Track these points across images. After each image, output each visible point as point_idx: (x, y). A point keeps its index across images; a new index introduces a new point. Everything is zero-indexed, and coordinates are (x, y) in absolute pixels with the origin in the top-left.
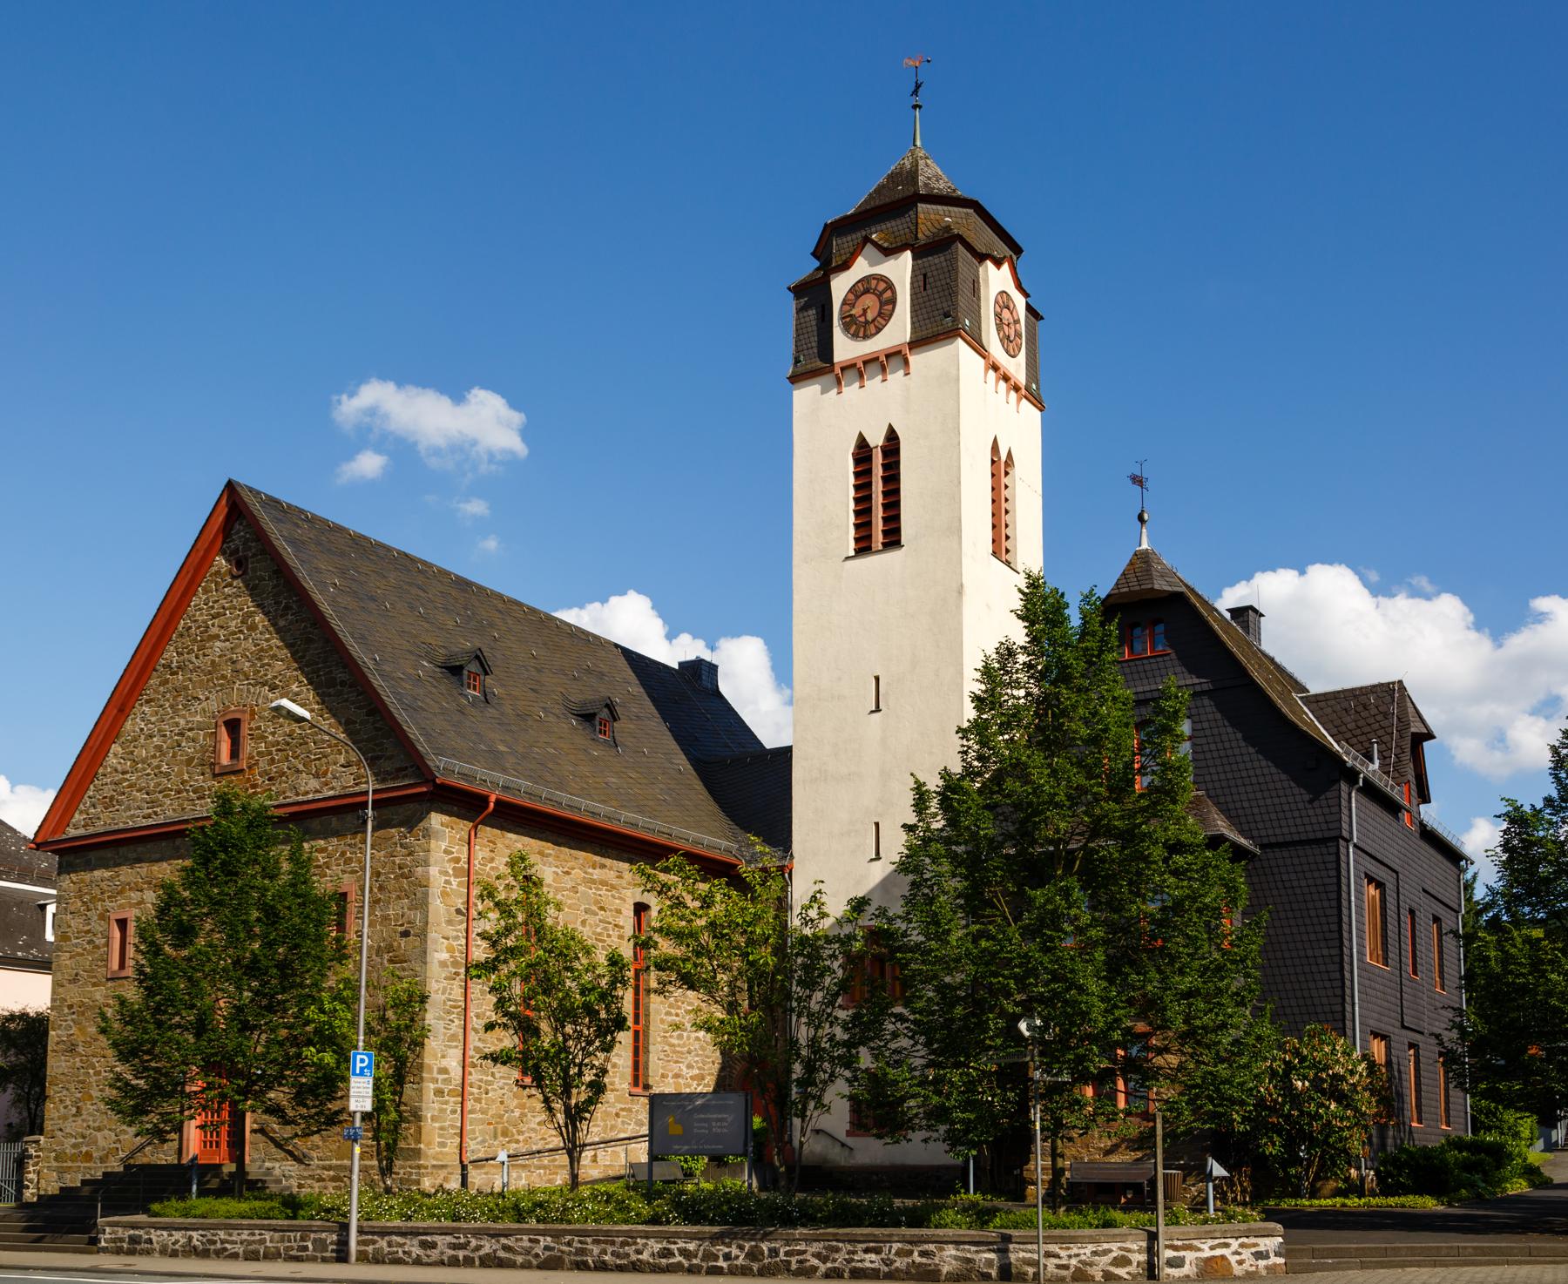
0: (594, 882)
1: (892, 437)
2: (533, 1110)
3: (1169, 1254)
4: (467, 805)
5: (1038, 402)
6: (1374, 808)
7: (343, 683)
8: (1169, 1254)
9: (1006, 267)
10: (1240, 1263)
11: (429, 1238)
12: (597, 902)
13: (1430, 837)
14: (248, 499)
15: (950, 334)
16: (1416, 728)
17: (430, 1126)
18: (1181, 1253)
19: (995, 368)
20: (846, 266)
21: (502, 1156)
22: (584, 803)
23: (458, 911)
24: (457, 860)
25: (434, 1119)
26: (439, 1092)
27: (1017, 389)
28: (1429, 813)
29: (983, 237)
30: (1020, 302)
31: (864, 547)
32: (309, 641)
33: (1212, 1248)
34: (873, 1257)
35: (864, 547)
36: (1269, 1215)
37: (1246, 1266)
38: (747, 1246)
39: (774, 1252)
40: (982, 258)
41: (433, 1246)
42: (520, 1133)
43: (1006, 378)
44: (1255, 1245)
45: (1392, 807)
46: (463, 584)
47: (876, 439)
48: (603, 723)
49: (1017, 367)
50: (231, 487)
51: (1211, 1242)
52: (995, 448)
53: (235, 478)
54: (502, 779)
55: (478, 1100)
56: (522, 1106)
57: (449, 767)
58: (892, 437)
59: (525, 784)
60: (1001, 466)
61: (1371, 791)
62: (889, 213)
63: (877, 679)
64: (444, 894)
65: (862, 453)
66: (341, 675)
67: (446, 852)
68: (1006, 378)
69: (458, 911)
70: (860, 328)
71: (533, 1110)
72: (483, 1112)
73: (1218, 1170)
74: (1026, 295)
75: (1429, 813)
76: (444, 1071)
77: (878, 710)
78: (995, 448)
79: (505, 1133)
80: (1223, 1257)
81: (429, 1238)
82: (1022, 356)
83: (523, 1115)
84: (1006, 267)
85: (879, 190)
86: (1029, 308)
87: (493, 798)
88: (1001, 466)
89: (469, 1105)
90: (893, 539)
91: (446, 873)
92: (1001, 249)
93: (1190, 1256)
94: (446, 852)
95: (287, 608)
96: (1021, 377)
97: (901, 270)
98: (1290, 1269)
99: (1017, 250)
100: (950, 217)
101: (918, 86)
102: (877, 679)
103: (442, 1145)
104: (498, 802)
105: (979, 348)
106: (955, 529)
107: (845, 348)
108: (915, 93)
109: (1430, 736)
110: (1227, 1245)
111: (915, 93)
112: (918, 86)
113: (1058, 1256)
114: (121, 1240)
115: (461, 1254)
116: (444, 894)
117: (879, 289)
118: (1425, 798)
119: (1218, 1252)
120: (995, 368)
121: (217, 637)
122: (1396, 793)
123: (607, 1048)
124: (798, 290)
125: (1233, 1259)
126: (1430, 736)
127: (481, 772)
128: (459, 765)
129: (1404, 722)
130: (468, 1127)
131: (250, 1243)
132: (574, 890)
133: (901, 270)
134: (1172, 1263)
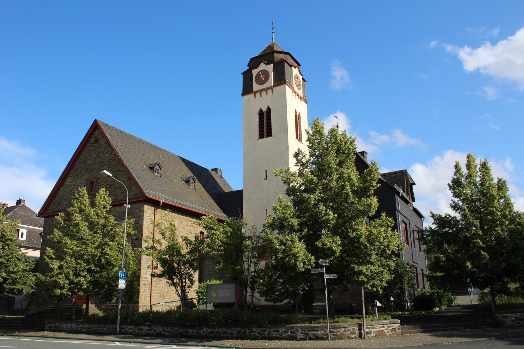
0: (189, 226)
1: (269, 109)
2: (171, 290)
3: (367, 330)
4: (155, 204)
5: (306, 101)
6: (403, 202)
7: (122, 171)
8: (367, 330)
9: (297, 68)
10: (388, 332)
11: (505, 315)
12: (189, 231)
13: (415, 210)
14: (99, 123)
15: (284, 83)
16: (411, 182)
17: (141, 294)
18: (371, 330)
19: (295, 92)
20: (257, 67)
21: (162, 303)
22: (186, 204)
23: (151, 233)
24: (151, 219)
25: (143, 292)
26: (145, 284)
27: (301, 98)
28: (415, 205)
29: (291, 62)
30: (301, 77)
31: (261, 136)
32: (114, 160)
33: (379, 328)
34: (276, 333)
35: (261, 136)
36: (394, 317)
37: (390, 333)
38: (237, 330)
39: (245, 332)
40: (291, 66)
41: (142, 330)
42: (168, 296)
43: (298, 95)
44: (392, 326)
45: (407, 202)
46: (156, 147)
47: (264, 110)
48: (192, 183)
49: (300, 92)
50: (95, 121)
51: (379, 326)
52: (296, 112)
53: (97, 119)
54: (164, 196)
55: (156, 287)
56: (168, 289)
57: (150, 193)
58: (269, 109)
59: (170, 198)
60: (297, 118)
61: (402, 198)
62: (268, 55)
63: (266, 171)
64: (148, 228)
65: (261, 113)
66: (121, 169)
67: (148, 216)
68: (298, 95)
69: (151, 233)
70: (260, 82)
71: (171, 290)
72: (157, 290)
73: (379, 304)
74: (302, 76)
75: (415, 205)
76: (146, 278)
77: (266, 179)
78: (296, 112)
79: (163, 297)
80: (383, 330)
81: (505, 315)
82: (301, 90)
83: (168, 291)
84: (297, 68)
85: (264, 50)
86: (303, 79)
87: (162, 202)
88: (297, 118)
89: (153, 288)
90: (269, 134)
91: (148, 222)
92: (295, 64)
93: (373, 330)
94: (148, 216)
95: (108, 151)
96: (302, 95)
97: (270, 68)
98: (403, 333)
99: (299, 65)
100: (283, 56)
101: (273, 28)
102: (266, 171)
103: (145, 299)
104: (163, 203)
105: (291, 87)
106: (286, 131)
107: (256, 87)
108: (273, 29)
109: (414, 184)
110: (384, 327)
111: (273, 29)
112: (273, 28)
113: (334, 332)
114: (52, 327)
115: (150, 332)
116: (148, 228)
117: (266, 73)
118: (414, 200)
119: (381, 329)
120: (295, 92)
121: (89, 159)
122: (408, 198)
123: (204, 227)
124: (244, 74)
125: (386, 331)
126: (414, 184)
127: (159, 195)
128: (152, 193)
129: (408, 181)
130: (153, 294)
131: (89, 328)
132: (183, 228)
133: (270, 68)
134: (367, 333)
